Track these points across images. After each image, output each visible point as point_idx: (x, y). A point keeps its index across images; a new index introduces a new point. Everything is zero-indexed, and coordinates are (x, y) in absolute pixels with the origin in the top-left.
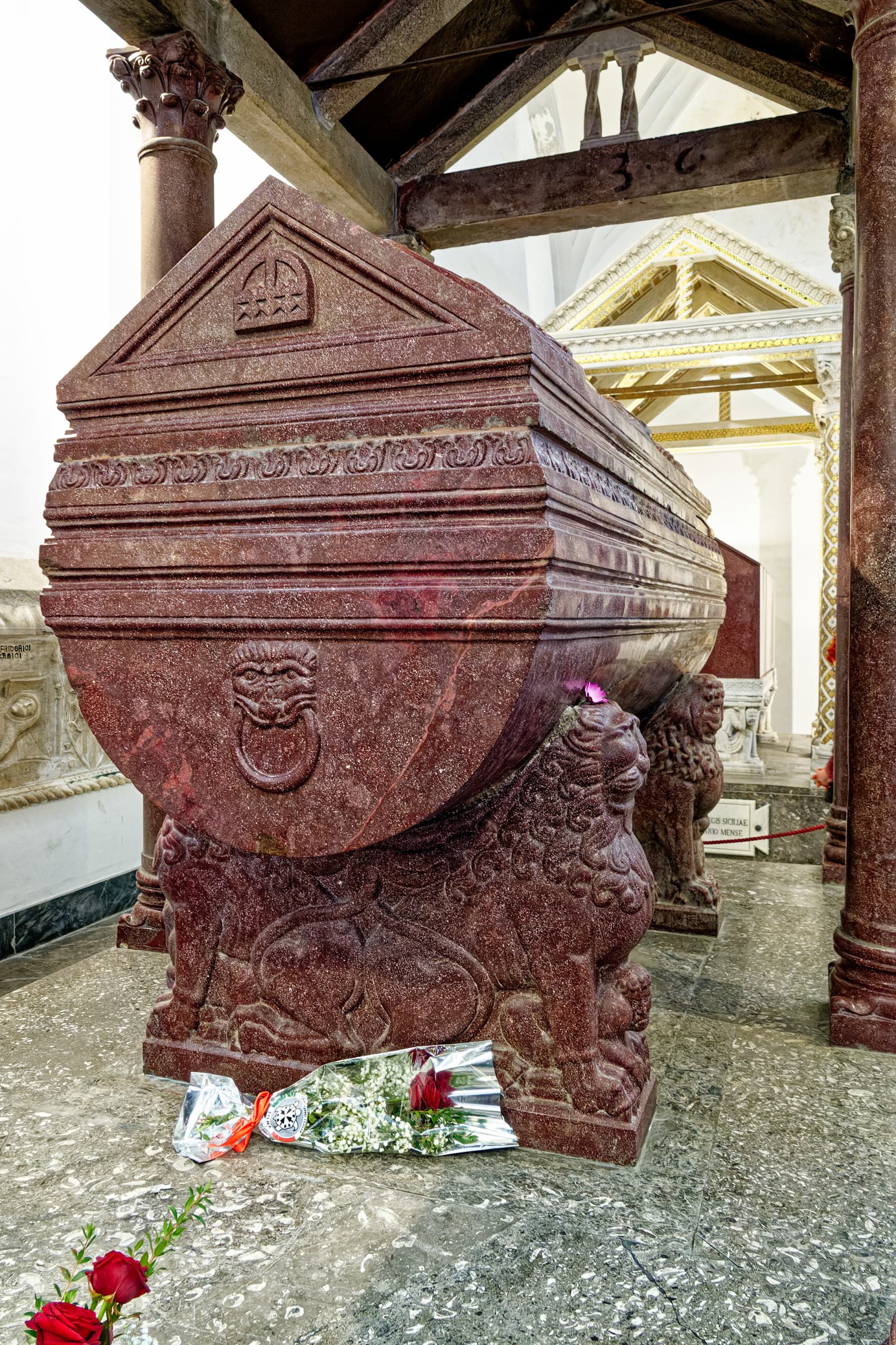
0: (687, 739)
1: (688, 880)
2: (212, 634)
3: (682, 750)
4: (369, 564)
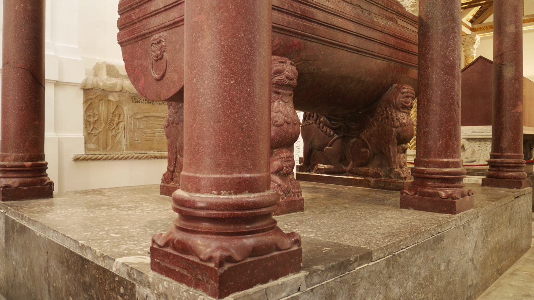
0: (394, 110)
1: (394, 169)
2: (147, 36)
3: (391, 114)
4: (169, 5)
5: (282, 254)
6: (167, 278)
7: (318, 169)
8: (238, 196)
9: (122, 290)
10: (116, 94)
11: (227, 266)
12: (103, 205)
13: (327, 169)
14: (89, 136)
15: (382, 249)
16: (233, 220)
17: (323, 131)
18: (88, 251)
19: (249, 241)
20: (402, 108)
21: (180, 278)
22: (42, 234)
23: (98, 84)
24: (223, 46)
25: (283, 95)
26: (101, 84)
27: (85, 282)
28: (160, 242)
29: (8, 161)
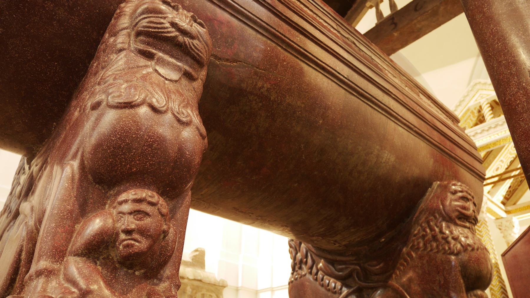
3: (441, 232)
17: (322, 286)
20: (459, 218)
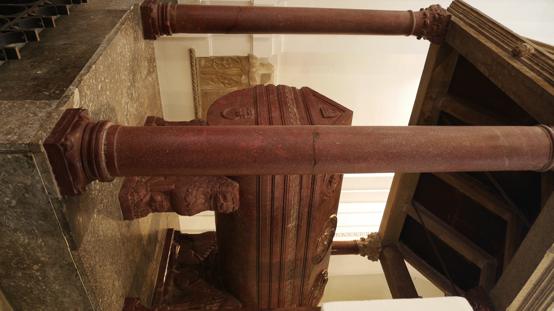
3: (216, 302)
5: (71, 182)
6: (60, 117)
7: (176, 246)
8: (103, 155)
9: (57, 92)
10: (247, 81)
11: (62, 148)
12: (134, 75)
13: (175, 253)
14: (211, 60)
15: (80, 259)
16: (89, 152)
18: (87, 71)
19: (79, 165)
21: (58, 125)
22: (106, 39)
23: (253, 67)
24: (187, 146)
25: (210, 202)
26: (254, 70)
27: (67, 69)
28: (83, 114)
29: (170, 10)
